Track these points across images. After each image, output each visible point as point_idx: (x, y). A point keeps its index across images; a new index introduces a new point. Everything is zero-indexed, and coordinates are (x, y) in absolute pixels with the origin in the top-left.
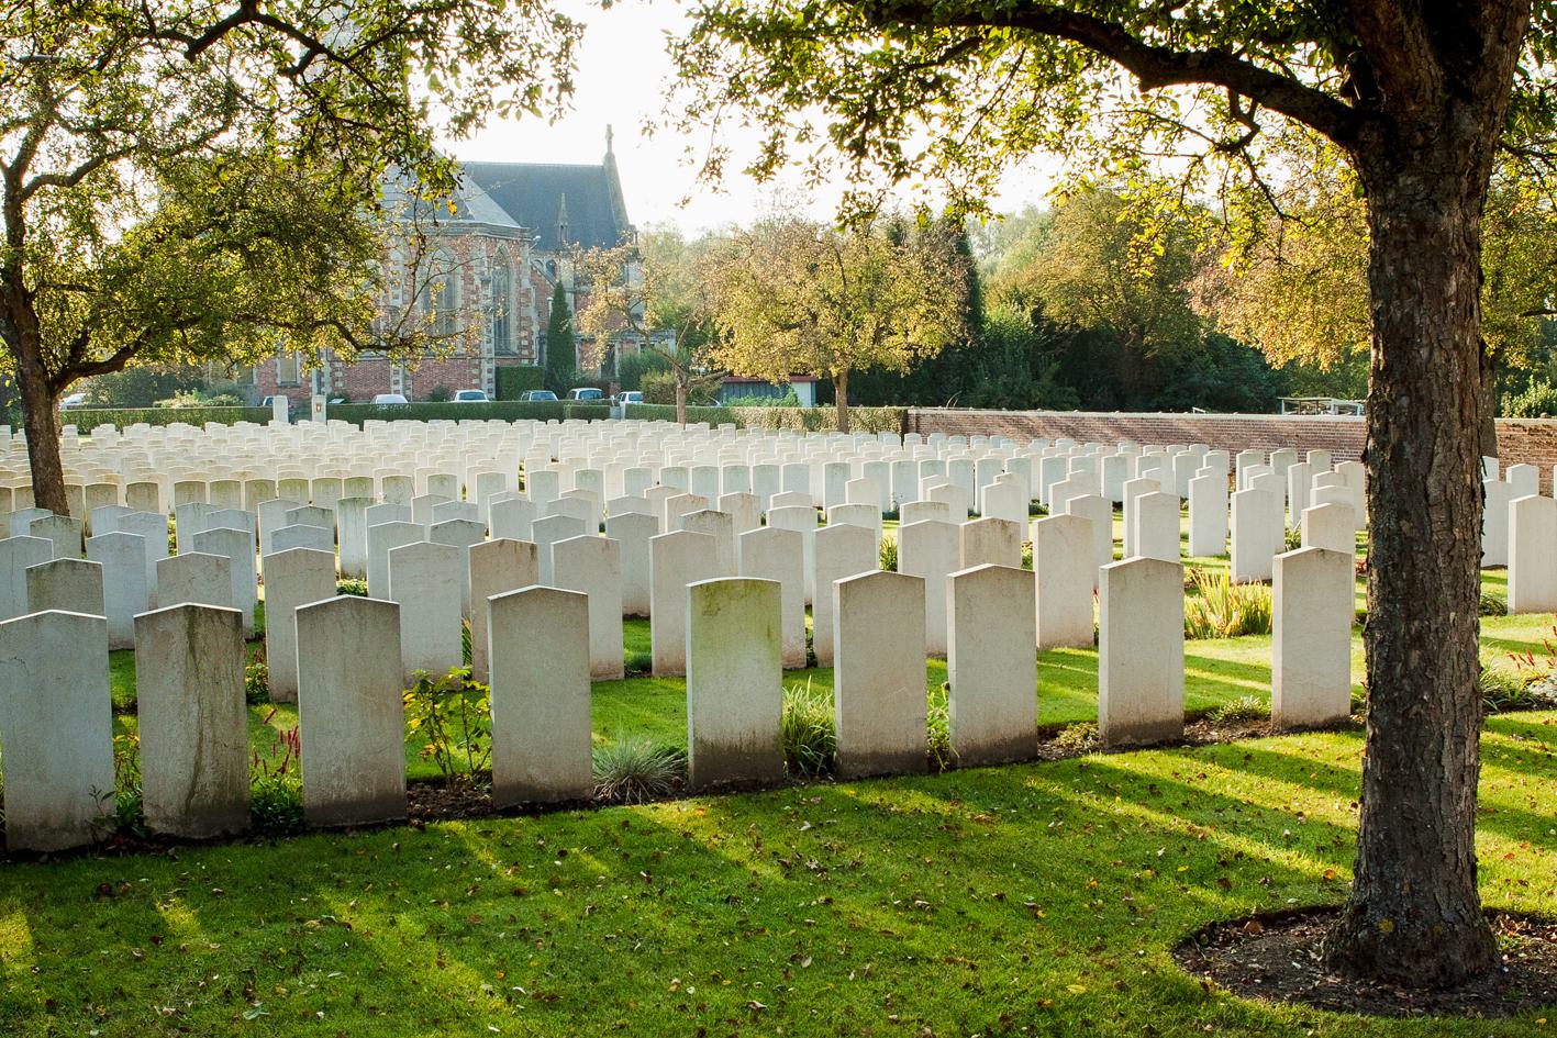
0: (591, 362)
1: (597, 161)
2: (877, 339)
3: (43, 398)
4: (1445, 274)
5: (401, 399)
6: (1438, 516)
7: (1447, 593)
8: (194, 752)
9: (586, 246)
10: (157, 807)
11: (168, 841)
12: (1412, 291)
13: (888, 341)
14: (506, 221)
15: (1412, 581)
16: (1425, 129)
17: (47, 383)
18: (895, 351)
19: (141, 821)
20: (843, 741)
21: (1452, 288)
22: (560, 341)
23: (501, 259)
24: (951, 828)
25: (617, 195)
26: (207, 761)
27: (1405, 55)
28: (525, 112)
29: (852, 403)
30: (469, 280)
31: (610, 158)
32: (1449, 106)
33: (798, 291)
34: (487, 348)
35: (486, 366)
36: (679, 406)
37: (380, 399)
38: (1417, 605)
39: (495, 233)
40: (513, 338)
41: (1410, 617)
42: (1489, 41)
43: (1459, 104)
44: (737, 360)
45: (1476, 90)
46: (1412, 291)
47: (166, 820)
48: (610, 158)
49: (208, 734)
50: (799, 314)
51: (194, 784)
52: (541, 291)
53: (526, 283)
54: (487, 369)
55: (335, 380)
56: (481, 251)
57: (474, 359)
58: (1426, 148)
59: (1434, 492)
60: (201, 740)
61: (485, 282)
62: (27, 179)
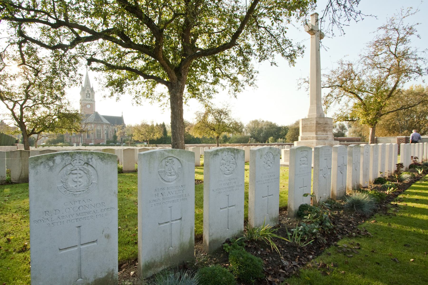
0: (119, 139)
1: (120, 116)
2: (153, 136)
3: (26, 137)
4: (178, 101)
5: (93, 144)
6: (178, 129)
7: (179, 139)
8: (21, 171)
9: (117, 125)
10: (14, 179)
11: (15, 183)
12: (174, 103)
13: (154, 137)
14: (108, 123)
15: (175, 137)
16: (175, 84)
17: (27, 135)
18: (155, 137)
19: (11, 181)
20: (124, 169)
21: (179, 103)
22: (115, 137)
23: (108, 127)
24: (131, 176)
25: (123, 120)
26: (23, 172)
27: (172, 74)
28: (75, 86)
29: (150, 144)
30: (103, 129)
31: (122, 116)
32: (178, 81)
33: (143, 130)
34: (105, 138)
35: (105, 140)
36: (129, 145)
37: (90, 144)
38: (176, 140)
39: (107, 124)
40: (109, 136)
41: (175, 141)
42: (183, 74)
43: (179, 81)
44: (136, 138)
45: (181, 80)
46: (174, 103)
47: (15, 180)
48: (122, 116)
49: (23, 168)
50: (143, 133)
51: (21, 175)
52: (113, 131)
53: (111, 130)
54: (105, 141)
55: (84, 142)
56: (105, 126)
57: (103, 139)
58: (175, 86)
59: (177, 126)
60: (22, 169)
61: (105, 130)
62: (24, 107)
